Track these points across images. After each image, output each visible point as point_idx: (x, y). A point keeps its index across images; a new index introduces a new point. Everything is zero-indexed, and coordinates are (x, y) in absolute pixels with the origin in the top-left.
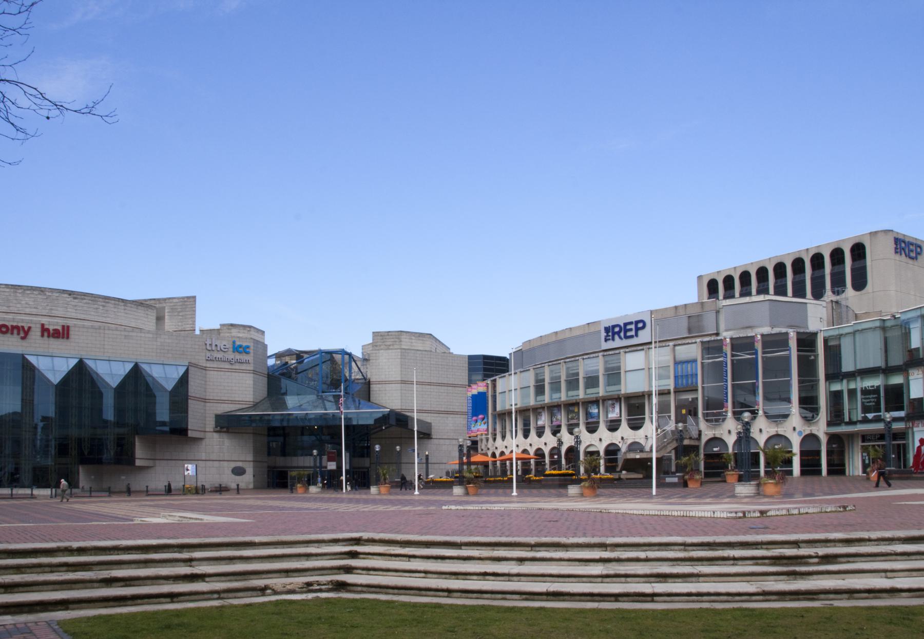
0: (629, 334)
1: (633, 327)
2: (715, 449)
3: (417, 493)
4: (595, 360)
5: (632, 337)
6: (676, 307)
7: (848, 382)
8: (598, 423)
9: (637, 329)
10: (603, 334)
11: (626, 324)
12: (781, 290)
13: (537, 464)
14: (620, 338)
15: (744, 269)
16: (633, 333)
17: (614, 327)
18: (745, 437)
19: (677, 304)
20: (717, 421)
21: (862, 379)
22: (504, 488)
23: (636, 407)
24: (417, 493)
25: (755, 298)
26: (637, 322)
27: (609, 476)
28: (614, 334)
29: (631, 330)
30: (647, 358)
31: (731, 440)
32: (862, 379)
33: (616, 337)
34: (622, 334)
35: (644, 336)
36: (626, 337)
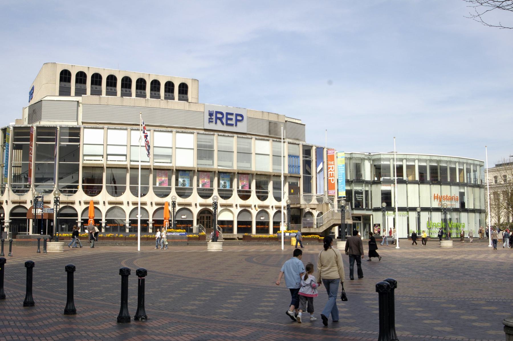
0: (229, 122)
1: (234, 117)
2: (262, 218)
3: (31, 233)
4: (231, 139)
5: (232, 125)
7: (371, 186)
9: (237, 121)
10: (207, 117)
11: (228, 114)
14: (223, 124)
16: (233, 122)
17: (217, 112)
18: (115, 206)
20: (71, 192)
23: (262, 181)
24: (398, 247)
25: (73, 98)
26: (237, 115)
27: (241, 236)
28: (217, 118)
29: (231, 119)
30: (129, 137)
31: (104, 209)
33: (218, 121)
34: (224, 120)
35: (241, 127)
36: (228, 124)
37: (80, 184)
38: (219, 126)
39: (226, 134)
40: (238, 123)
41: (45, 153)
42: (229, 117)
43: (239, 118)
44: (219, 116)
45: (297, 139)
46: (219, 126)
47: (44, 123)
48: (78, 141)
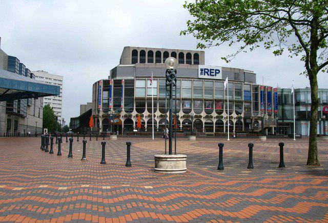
1: (214, 71)
3: (228, 139)
6: (231, 68)
8: (180, 109)
9: (216, 73)
10: (200, 72)
11: (211, 70)
12: (189, 63)
13: (148, 126)
14: (208, 75)
15: (143, 49)
16: (214, 74)
17: (205, 69)
19: (232, 67)
21: (305, 102)
22: (224, 138)
24: (228, 139)
26: (216, 70)
28: (205, 72)
32: (305, 102)
33: (206, 74)
34: (209, 73)
36: (211, 75)
37: (135, 108)
38: (206, 76)
39: (141, 79)
40: (217, 74)
41: (118, 93)
42: (212, 71)
43: (217, 72)
44: (206, 71)
45: (251, 82)
46: (206, 76)
47: (118, 78)
48: (133, 86)
